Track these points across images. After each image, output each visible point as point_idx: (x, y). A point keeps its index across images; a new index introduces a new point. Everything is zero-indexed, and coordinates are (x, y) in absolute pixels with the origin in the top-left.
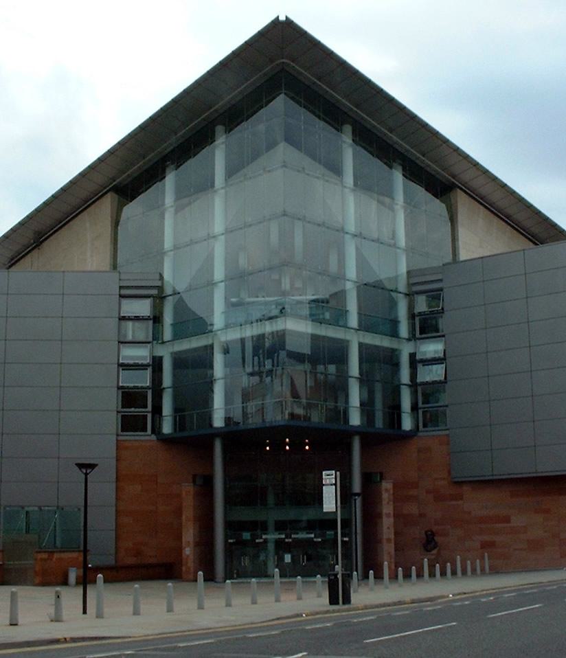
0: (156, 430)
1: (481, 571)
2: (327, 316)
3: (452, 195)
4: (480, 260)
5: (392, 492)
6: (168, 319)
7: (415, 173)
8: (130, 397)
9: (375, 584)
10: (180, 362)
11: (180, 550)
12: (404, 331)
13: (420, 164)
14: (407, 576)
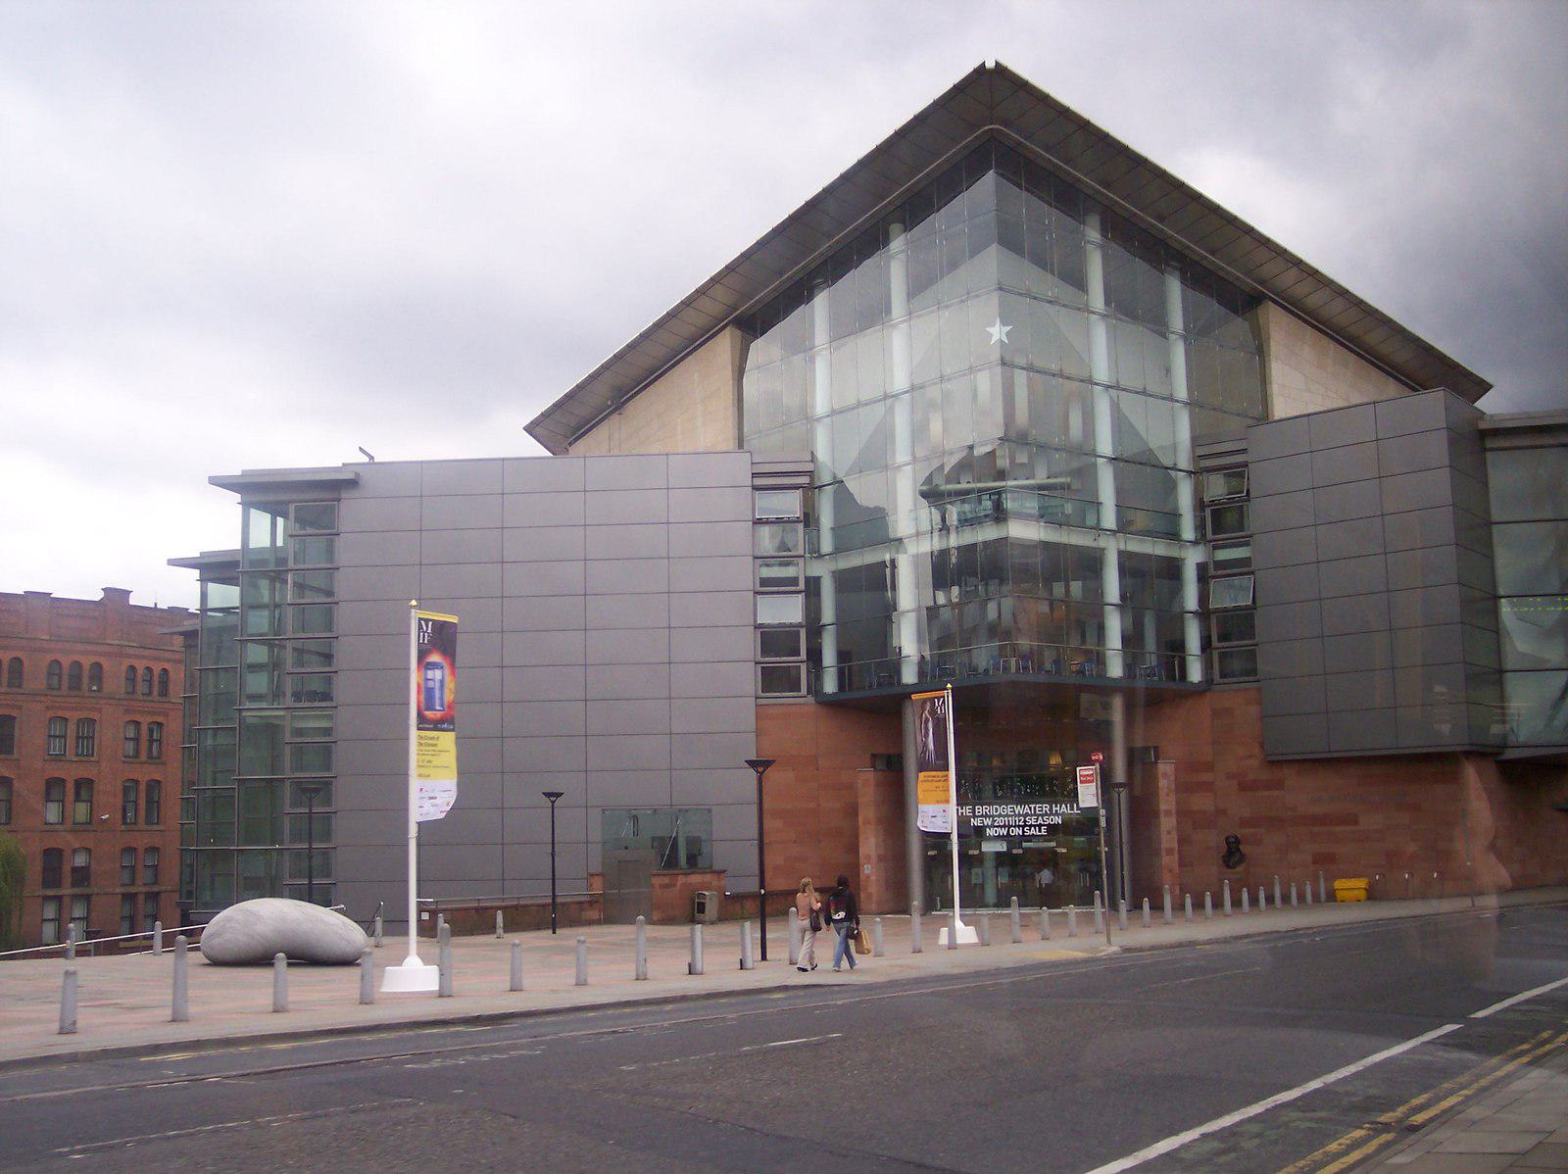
0: (815, 687)
1: (1282, 899)
2: (1069, 509)
3: (1261, 311)
4: (1306, 418)
5: (1173, 778)
6: (826, 520)
7: (1200, 278)
8: (774, 640)
9: (1129, 919)
10: (845, 581)
11: (856, 867)
12: (1188, 532)
13: (1209, 266)
14: (1199, 905)
